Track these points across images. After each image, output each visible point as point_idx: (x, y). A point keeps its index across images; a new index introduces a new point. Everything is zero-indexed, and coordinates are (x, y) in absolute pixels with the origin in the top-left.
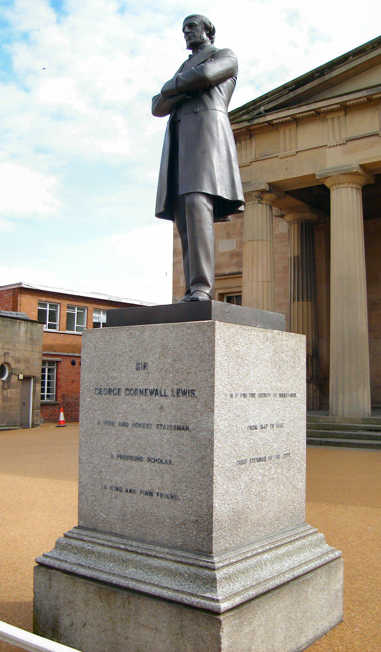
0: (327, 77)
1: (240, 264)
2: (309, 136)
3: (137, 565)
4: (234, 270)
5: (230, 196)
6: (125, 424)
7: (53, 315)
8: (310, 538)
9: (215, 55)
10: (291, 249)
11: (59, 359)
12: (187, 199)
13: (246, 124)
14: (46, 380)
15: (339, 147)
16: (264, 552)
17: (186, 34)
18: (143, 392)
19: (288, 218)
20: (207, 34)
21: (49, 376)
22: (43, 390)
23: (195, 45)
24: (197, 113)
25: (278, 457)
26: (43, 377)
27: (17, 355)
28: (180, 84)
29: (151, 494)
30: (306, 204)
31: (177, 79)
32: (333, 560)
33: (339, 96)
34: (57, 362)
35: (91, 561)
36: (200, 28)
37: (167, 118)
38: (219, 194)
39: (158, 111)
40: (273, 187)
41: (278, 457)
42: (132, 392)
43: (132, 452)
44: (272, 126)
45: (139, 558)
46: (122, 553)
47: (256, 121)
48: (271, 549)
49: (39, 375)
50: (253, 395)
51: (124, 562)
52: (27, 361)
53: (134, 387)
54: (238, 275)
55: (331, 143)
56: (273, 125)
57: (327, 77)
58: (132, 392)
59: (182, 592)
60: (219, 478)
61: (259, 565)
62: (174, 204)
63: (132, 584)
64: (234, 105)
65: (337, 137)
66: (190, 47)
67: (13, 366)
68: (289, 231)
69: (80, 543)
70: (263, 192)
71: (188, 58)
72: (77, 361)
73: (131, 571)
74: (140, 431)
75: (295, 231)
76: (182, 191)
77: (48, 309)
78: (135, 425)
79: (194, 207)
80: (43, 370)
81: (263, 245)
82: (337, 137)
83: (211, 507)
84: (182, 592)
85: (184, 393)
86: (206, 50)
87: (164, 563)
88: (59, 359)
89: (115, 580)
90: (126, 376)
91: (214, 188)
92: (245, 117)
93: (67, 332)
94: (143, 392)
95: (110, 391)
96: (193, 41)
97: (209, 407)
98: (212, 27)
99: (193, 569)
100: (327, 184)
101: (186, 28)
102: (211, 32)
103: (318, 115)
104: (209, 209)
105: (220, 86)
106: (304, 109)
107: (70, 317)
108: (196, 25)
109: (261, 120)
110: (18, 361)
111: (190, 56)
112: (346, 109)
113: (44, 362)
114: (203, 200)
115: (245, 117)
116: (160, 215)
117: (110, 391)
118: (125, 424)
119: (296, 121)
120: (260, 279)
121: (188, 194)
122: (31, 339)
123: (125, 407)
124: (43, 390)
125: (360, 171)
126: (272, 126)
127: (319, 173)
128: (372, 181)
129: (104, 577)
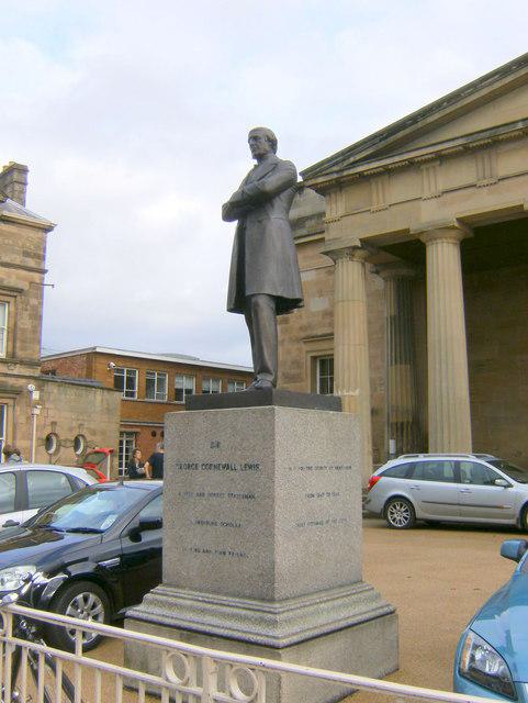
0: (420, 125)
1: (331, 324)
2: (400, 190)
3: (213, 613)
4: (326, 330)
6: (202, 495)
7: (131, 382)
8: (366, 594)
9: (276, 165)
10: (387, 309)
11: (138, 430)
12: (253, 300)
13: (335, 176)
14: (124, 454)
15: (434, 200)
16: (321, 602)
17: (251, 146)
18: (217, 467)
19: (383, 274)
21: (127, 450)
22: (121, 465)
23: (259, 156)
25: (335, 521)
26: (121, 450)
27: (92, 427)
28: (245, 196)
29: (224, 553)
30: (401, 259)
31: (242, 192)
32: (387, 614)
33: (434, 144)
34: (136, 433)
35: (175, 613)
36: (263, 140)
37: (235, 224)
40: (366, 243)
41: (335, 521)
42: (208, 466)
43: (208, 518)
44: (363, 179)
45: (215, 607)
46: (199, 604)
47: (345, 173)
48: (328, 600)
49: (117, 448)
50: (310, 468)
51: (203, 611)
52: (103, 433)
53: (209, 462)
54: (329, 337)
55: (426, 194)
56: (364, 177)
57: (420, 125)
58: (208, 466)
59: (250, 633)
60: (279, 538)
61: (317, 612)
62: (240, 301)
63: (208, 629)
64: (294, 214)
65: (433, 189)
67: (88, 439)
68: (386, 287)
69: (165, 598)
70: (355, 248)
72: (158, 432)
73: (208, 619)
74: (215, 501)
75: (391, 285)
76: (248, 293)
77: (125, 375)
78: (210, 495)
79: (257, 305)
80: (121, 443)
81: (351, 305)
82: (433, 189)
83: (273, 563)
84: (250, 633)
85: (250, 467)
86: (270, 161)
87: (235, 611)
88: (138, 430)
89: (194, 626)
90: (202, 454)
92: (335, 168)
93: (146, 400)
94: (217, 467)
95: (189, 466)
97: (271, 478)
99: (258, 614)
100: (423, 239)
102: (273, 143)
103: (412, 166)
105: (281, 196)
106: (397, 159)
107: (150, 383)
109: (352, 171)
110: (94, 433)
112: (441, 158)
113: (122, 433)
115: (335, 168)
116: (230, 310)
117: (189, 466)
118: (202, 495)
119: (388, 172)
120: (346, 347)
121: (253, 295)
122: (107, 409)
123: (201, 479)
124: (121, 465)
125: (456, 225)
126: (363, 179)
127: (414, 227)
128: (471, 235)
129: (186, 624)
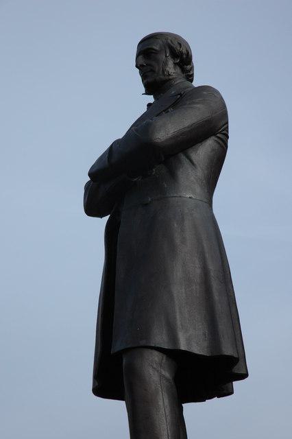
5: (205, 344)
20: (175, 64)
24: (146, 205)
37: (107, 218)
38: (183, 346)
39: (92, 208)
66: (150, 88)
71: (145, 109)
91: (174, 338)
96: (150, 80)
98: (184, 51)
101: (140, 57)
102: (184, 60)
104: (161, 376)
108: (156, 52)
111: (149, 105)
114: (156, 357)
